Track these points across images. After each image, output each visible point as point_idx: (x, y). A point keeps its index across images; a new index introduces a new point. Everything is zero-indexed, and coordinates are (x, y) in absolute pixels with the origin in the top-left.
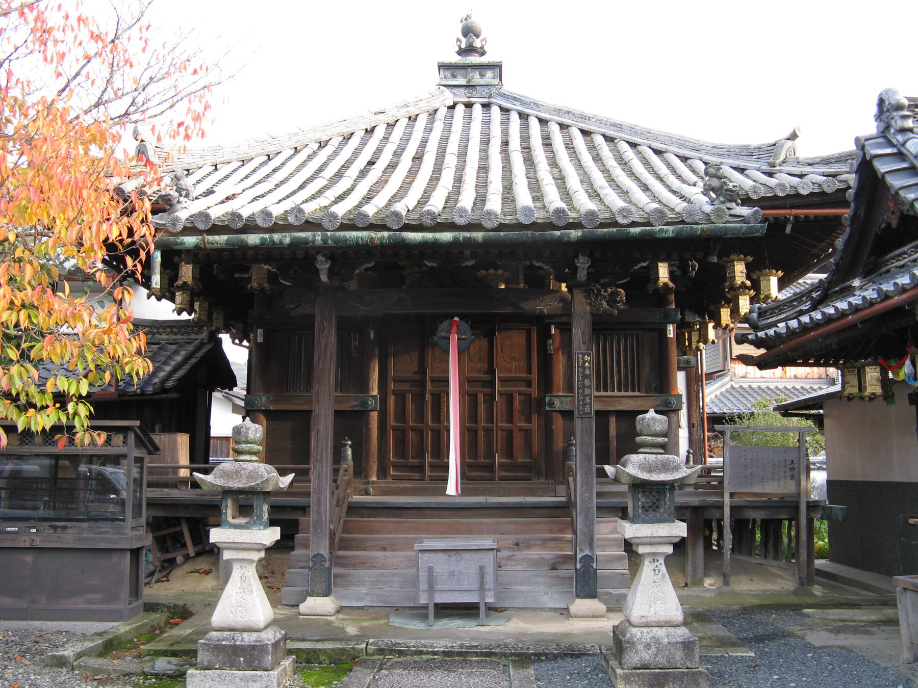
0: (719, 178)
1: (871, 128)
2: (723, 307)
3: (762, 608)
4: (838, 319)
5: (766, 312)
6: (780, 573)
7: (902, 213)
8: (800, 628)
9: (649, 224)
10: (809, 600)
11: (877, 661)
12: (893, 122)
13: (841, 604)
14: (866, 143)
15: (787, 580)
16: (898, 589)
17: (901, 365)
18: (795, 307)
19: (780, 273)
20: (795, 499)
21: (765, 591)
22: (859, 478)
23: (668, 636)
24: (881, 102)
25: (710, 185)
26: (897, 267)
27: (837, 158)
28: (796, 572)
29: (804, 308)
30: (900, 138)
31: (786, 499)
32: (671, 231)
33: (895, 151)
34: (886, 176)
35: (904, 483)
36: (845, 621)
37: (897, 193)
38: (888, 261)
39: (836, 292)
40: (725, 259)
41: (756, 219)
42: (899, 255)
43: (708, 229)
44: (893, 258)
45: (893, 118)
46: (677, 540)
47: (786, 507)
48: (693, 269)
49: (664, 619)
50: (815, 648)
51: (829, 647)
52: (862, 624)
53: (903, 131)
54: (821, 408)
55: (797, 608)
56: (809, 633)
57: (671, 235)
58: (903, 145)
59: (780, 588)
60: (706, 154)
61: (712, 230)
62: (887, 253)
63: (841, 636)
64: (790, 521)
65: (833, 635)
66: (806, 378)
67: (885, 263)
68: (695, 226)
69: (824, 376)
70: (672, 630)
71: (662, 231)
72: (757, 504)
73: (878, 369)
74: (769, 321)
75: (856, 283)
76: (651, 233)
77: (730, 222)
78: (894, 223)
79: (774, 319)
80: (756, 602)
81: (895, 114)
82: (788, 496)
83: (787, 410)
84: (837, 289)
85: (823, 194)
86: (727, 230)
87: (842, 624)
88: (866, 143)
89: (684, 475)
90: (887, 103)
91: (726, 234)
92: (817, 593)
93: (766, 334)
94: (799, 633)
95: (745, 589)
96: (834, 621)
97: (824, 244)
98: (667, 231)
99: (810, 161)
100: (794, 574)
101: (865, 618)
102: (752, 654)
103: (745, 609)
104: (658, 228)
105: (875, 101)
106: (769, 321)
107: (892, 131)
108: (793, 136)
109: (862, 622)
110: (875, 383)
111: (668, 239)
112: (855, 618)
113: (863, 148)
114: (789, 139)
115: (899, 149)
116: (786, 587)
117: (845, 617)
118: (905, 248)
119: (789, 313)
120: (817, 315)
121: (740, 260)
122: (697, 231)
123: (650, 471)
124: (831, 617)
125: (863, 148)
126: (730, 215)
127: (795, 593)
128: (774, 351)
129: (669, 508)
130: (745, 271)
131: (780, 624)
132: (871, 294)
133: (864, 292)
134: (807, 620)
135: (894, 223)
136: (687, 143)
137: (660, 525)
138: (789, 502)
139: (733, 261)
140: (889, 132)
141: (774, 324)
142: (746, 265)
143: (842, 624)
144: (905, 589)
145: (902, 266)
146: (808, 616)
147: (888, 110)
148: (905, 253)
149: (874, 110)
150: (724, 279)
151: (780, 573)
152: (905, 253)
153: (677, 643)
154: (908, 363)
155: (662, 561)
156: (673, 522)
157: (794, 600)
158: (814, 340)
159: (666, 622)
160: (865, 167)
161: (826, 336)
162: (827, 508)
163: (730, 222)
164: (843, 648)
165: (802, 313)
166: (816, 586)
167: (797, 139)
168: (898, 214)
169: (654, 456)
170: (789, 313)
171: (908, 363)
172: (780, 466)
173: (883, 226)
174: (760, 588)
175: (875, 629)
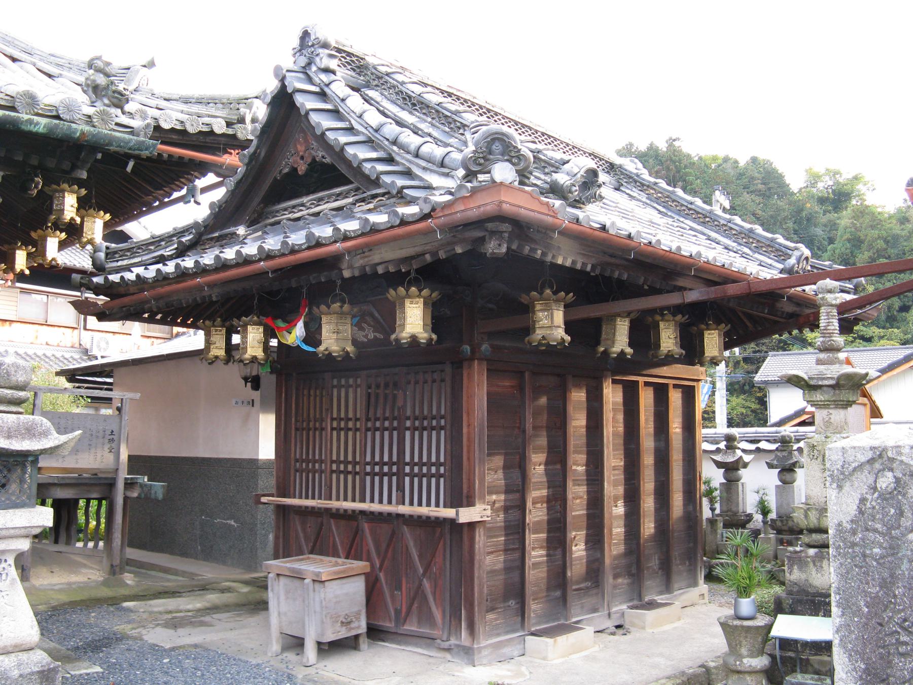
0: (107, 75)
1: (288, 62)
2: (20, 248)
3: (73, 605)
4: (237, 265)
5: (116, 253)
6: (85, 562)
7: (314, 159)
8: (130, 626)
9: (13, 108)
10: (125, 592)
11: (243, 658)
12: (317, 59)
13: (166, 593)
14: (288, 74)
15: (92, 568)
16: (270, 575)
17: (291, 325)
18: (152, 252)
19: (108, 217)
20: (110, 476)
21: (69, 584)
22: (153, 453)
23: (19, 665)
24: (305, 34)
25: (94, 81)
26: (290, 219)
27: (198, 99)
28: (105, 560)
29: (167, 252)
30: (324, 77)
31: (100, 475)
32: (42, 125)
33: (317, 89)
34: (311, 113)
35: (210, 459)
36: (171, 612)
37: (323, 134)
38: (278, 212)
39: (212, 239)
40: (55, 186)
41: (145, 133)
42: (294, 207)
43: (90, 133)
44: (285, 209)
45: (317, 55)
46: (38, 531)
47: (100, 484)
48: (36, 187)
49: (13, 642)
50: (165, 650)
51: (180, 647)
52: (190, 614)
53: (327, 70)
54: (111, 377)
55: (114, 602)
56: (144, 632)
57: (41, 129)
58: (327, 85)
59: (86, 579)
60: (41, 60)
61: (94, 136)
62: (279, 201)
63: (181, 631)
64: (100, 500)
65: (171, 632)
66: (58, 346)
67: (274, 214)
68: (74, 125)
69: (77, 345)
70: (24, 656)
71: (30, 122)
72: (68, 481)
73: (261, 329)
74: (120, 263)
75: (241, 230)
76: (15, 123)
77: (114, 130)
78: (302, 168)
79: (125, 262)
80: (64, 598)
81: (321, 51)
82: (101, 472)
83: (74, 375)
84: (216, 234)
85: (184, 132)
86: (111, 140)
87: (170, 616)
88: (288, 74)
89: (57, 443)
90: (313, 37)
91: (110, 144)
92: (129, 582)
93: (122, 278)
94: (134, 633)
95: (45, 583)
96: (160, 613)
97: (162, 192)
98: (37, 124)
99: (167, 97)
100: (101, 562)
101: (190, 607)
102: (98, 669)
103: (54, 608)
104: (26, 117)
105: (298, 33)
106: (120, 263)
107: (314, 68)
108: (151, 65)
109: (189, 611)
110: (257, 345)
111: (37, 134)
112: (181, 607)
113: (282, 80)
114: (145, 66)
115: (322, 89)
116: (93, 577)
117: (170, 608)
118: (305, 200)
119: (145, 258)
120: (188, 263)
121: (72, 192)
122: (75, 133)
123: (9, 437)
124: (156, 609)
125: (282, 80)
126: (117, 124)
127: (105, 583)
128: (118, 302)
129: (30, 488)
130: (76, 205)
131: (105, 623)
132: (251, 249)
133: (249, 245)
134: (133, 616)
135: (302, 168)
136: (16, 42)
137: (17, 511)
138: (105, 478)
139: (63, 191)
140: (310, 69)
141: (128, 268)
142: (78, 198)
143: (170, 616)
144: (278, 575)
145: (298, 219)
146: (129, 610)
147: (313, 45)
148: (303, 205)
149: (296, 43)
150: (50, 211)
151: (85, 562)
152: (303, 205)
153: (32, 673)
154: (300, 325)
155: (11, 561)
156: (33, 506)
157: (106, 592)
158: (200, 287)
159: (16, 646)
160: (283, 102)
161: (211, 285)
162: (146, 485)
163: (114, 130)
164: (196, 646)
165: (162, 260)
166: (126, 574)
167: (154, 69)
168: (309, 160)
169: (14, 415)
170: (145, 258)
171: (300, 325)
172: (97, 437)
173: (286, 170)
174: (63, 581)
175: (207, 619)
